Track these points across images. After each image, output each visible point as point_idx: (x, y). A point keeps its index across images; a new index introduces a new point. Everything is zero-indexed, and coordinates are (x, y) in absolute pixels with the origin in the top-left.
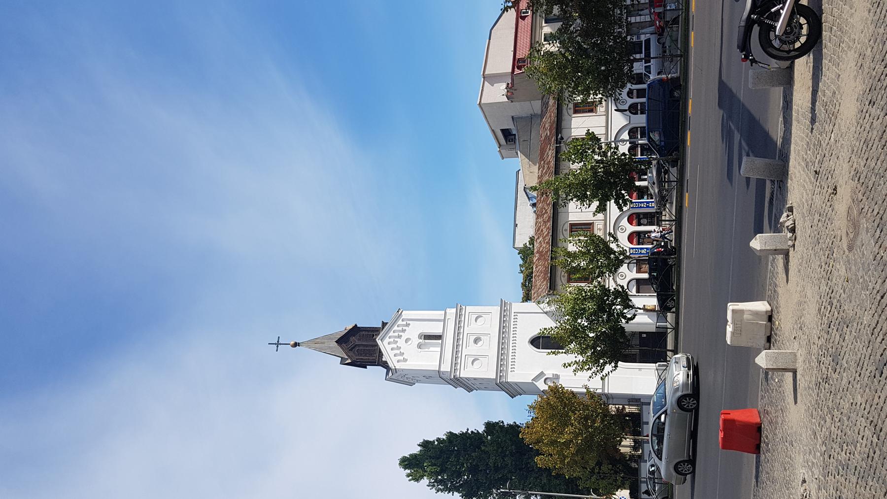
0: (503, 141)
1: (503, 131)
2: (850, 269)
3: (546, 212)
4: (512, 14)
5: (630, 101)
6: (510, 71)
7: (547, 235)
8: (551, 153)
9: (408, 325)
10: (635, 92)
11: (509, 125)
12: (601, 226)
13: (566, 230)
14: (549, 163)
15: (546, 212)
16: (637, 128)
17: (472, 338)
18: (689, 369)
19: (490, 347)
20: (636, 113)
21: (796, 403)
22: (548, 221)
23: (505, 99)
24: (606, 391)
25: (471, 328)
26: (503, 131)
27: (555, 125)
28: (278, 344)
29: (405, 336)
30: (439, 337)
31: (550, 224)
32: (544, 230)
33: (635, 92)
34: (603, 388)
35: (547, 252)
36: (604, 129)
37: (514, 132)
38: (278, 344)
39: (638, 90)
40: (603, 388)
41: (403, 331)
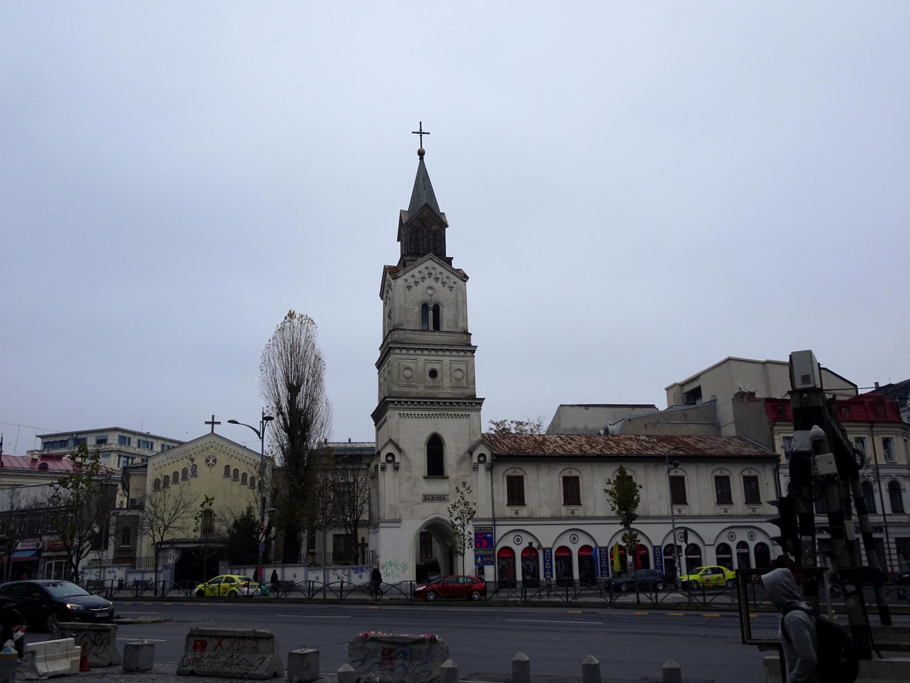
0: (688, 389)
2: (350, 499)
3: (592, 447)
5: (733, 545)
8: (664, 449)
9: (451, 288)
10: (745, 551)
11: (706, 397)
13: (570, 472)
14: (653, 448)
15: (592, 447)
16: (700, 554)
17: (436, 366)
18: (358, 469)
20: (718, 552)
21: (423, 230)
22: (581, 450)
28: (421, 133)
29: (438, 285)
30: (437, 327)
32: (570, 446)
33: (745, 551)
35: (543, 450)
36: (646, 514)
37: (698, 402)
38: (421, 133)
39: (747, 555)
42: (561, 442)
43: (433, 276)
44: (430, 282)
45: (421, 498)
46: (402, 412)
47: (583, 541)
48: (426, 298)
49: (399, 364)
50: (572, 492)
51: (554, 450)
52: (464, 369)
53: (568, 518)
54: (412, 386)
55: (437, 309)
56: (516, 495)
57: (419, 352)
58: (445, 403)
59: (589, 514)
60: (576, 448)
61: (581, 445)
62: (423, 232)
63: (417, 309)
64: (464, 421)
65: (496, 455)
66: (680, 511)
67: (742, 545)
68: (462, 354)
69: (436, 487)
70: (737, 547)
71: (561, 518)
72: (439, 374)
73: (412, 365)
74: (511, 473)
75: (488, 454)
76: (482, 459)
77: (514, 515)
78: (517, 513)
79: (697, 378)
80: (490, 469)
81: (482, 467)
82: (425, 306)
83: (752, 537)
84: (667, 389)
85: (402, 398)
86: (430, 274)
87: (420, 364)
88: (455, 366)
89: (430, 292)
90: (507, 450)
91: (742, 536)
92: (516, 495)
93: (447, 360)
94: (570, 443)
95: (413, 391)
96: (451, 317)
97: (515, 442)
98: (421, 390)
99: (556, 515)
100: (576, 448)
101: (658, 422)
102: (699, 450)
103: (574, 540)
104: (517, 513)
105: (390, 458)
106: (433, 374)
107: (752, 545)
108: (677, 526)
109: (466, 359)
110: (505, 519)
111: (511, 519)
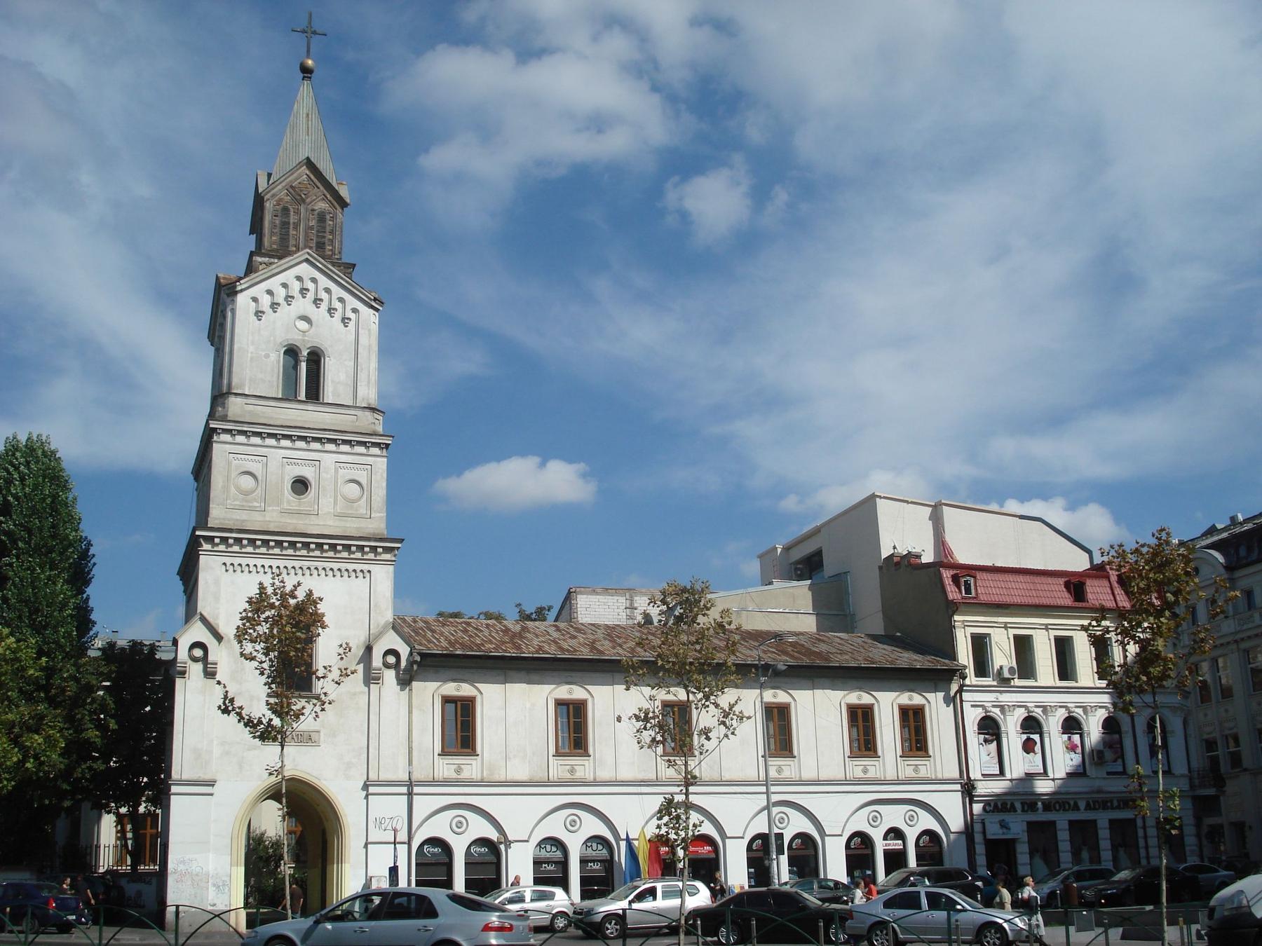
1: (819, 553)
4: (1079, 563)
5: (877, 835)
6: (983, 599)
7: (561, 649)
9: (345, 320)
12: (786, 774)
17: (308, 472)
19: (278, 514)
22: (592, 647)
23: (885, 553)
24: (174, 789)
25: (328, 466)
26: (819, 553)
27: (819, 662)
29: (320, 314)
30: (314, 393)
31: (585, 653)
32: (573, 642)
34: (182, 783)
35: (518, 648)
36: (716, 777)
40: (182, 783)
41: (331, 311)
42: (555, 635)
43: (310, 296)
44: (303, 305)
46: (228, 560)
47: (595, 827)
48: (295, 338)
49: (229, 463)
50: (574, 728)
51: (540, 648)
52: (364, 482)
53: (446, 782)
55: (315, 358)
56: (461, 730)
57: (272, 442)
58: (320, 546)
59: (604, 775)
60: (584, 645)
61: (594, 641)
62: (297, 212)
63: (276, 359)
64: (360, 584)
65: (422, 655)
66: (779, 771)
67: (895, 833)
68: (362, 449)
70: (885, 838)
71: (548, 783)
72: (312, 492)
73: (255, 467)
74: (451, 689)
75: (404, 651)
76: (391, 659)
77: (454, 775)
78: (458, 771)
79: (816, 531)
80: (405, 681)
81: (390, 675)
82: (292, 352)
83: (911, 820)
84: (760, 557)
85: (231, 531)
86: (304, 291)
87: (274, 465)
89: (303, 325)
90: (444, 644)
91: (894, 816)
92: (461, 730)
93: (329, 460)
94: (574, 637)
95: (255, 521)
96: (342, 377)
97: (465, 631)
98: (272, 518)
99: (542, 775)
100: (584, 645)
101: (743, 609)
102: (819, 655)
103: (572, 826)
104: (572, 771)
105: (198, 653)
106: (301, 485)
107: (912, 835)
108: (775, 798)
109: (370, 460)
110: (434, 782)
111: (446, 782)
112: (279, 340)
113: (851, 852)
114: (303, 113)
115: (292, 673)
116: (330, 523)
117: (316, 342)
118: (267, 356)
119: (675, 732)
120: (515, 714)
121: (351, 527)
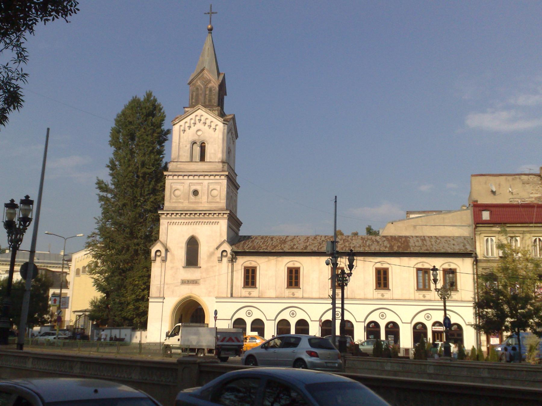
17: (198, 188)
24: (150, 300)
30: (202, 158)
34: (120, 332)
40: (120, 332)
44: (199, 126)
45: (180, 281)
46: (170, 221)
53: (289, 298)
54: (180, 202)
69: (192, 274)
78: (250, 294)
85: (170, 211)
88: (211, 187)
92: (250, 278)
93: (206, 182)
106: (196, 193)
112: (190, 140)
113: (416, 331)
114: (207, 48)
115: (192, 258)
116: (206, 205)
117: (202, 139)
118: (186, 146)
119: (339, 280)
120: (272, 271)
121: (213, 206)
